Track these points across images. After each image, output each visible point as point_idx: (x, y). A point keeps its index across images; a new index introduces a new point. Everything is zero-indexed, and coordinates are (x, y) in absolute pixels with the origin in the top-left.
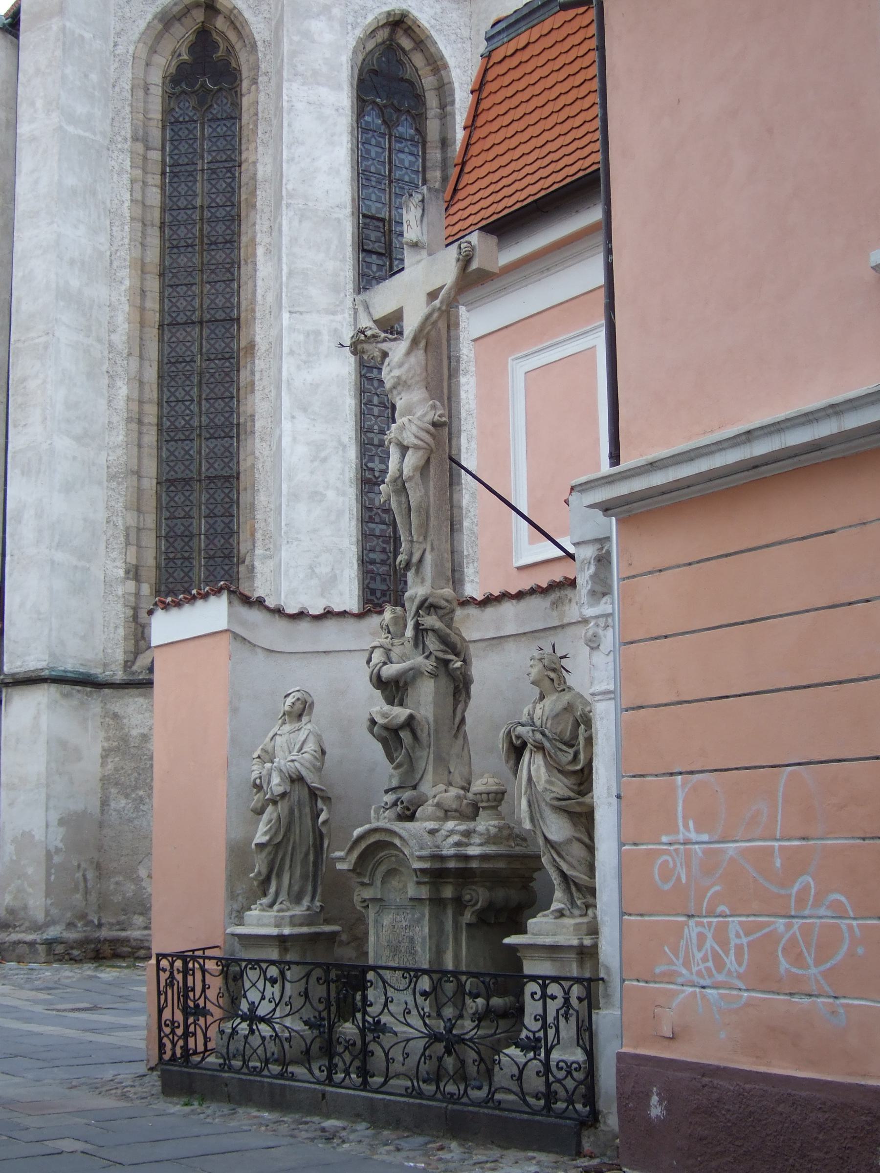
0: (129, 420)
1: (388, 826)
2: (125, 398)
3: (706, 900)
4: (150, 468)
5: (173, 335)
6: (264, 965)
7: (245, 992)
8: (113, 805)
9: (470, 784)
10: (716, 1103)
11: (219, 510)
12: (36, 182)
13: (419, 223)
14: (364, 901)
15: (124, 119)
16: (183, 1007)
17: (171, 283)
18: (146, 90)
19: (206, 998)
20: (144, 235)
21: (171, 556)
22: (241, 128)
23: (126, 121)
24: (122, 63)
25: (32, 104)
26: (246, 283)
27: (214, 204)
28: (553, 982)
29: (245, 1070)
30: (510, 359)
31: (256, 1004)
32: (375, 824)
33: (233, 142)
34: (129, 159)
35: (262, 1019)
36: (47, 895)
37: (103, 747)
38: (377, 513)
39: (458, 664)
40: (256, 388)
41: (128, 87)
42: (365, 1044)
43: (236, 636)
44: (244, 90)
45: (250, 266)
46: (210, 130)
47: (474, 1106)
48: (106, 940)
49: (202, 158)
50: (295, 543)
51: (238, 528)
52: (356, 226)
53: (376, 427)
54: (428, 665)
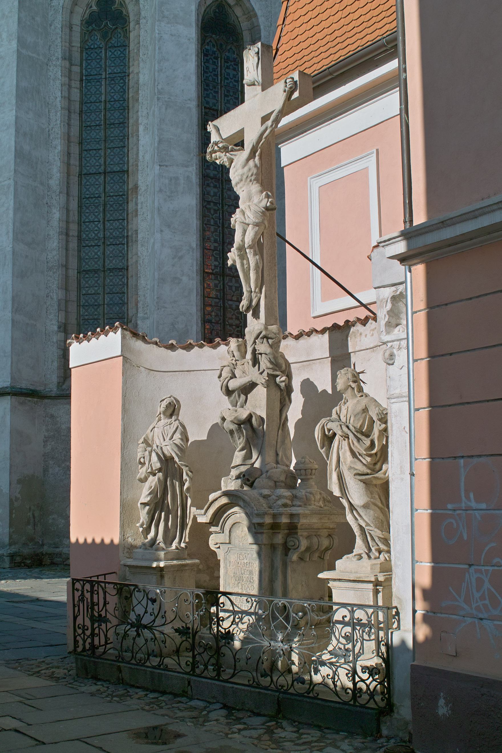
0: (61, 233)
2: (58, 220)
3: (484, 554)
5: (88, 181)
7: (133, 607)
8: (51, 471)
10: (493, 709)
13: (255, 68)
15: (57, 46)
16: (91, 616)
17: (86, 149)
18: (71, 28)
19: (106, 610)
22: (129, 52)
23: (58, 47)
26: (132, 149)
27: (112, 100)
28: (359, 608)
30: (309, 178)
31: (141, 616)
33: (124, 61)
34: (60, 71)
35: (145, 627)
36: (11, 526)
37: (45, 435)
40: (139, 214)
41: (59, 26)
42: (218, 648)
44: (131, 29)
45: (135, 138)
46: (110, 53)
47: (299, 696)
48: (46, 554)
49: (105, 71)
50: (163, 309)
51: (128, 300)
52: (200, 113)
53: (212, 239)
54: (261, 379)
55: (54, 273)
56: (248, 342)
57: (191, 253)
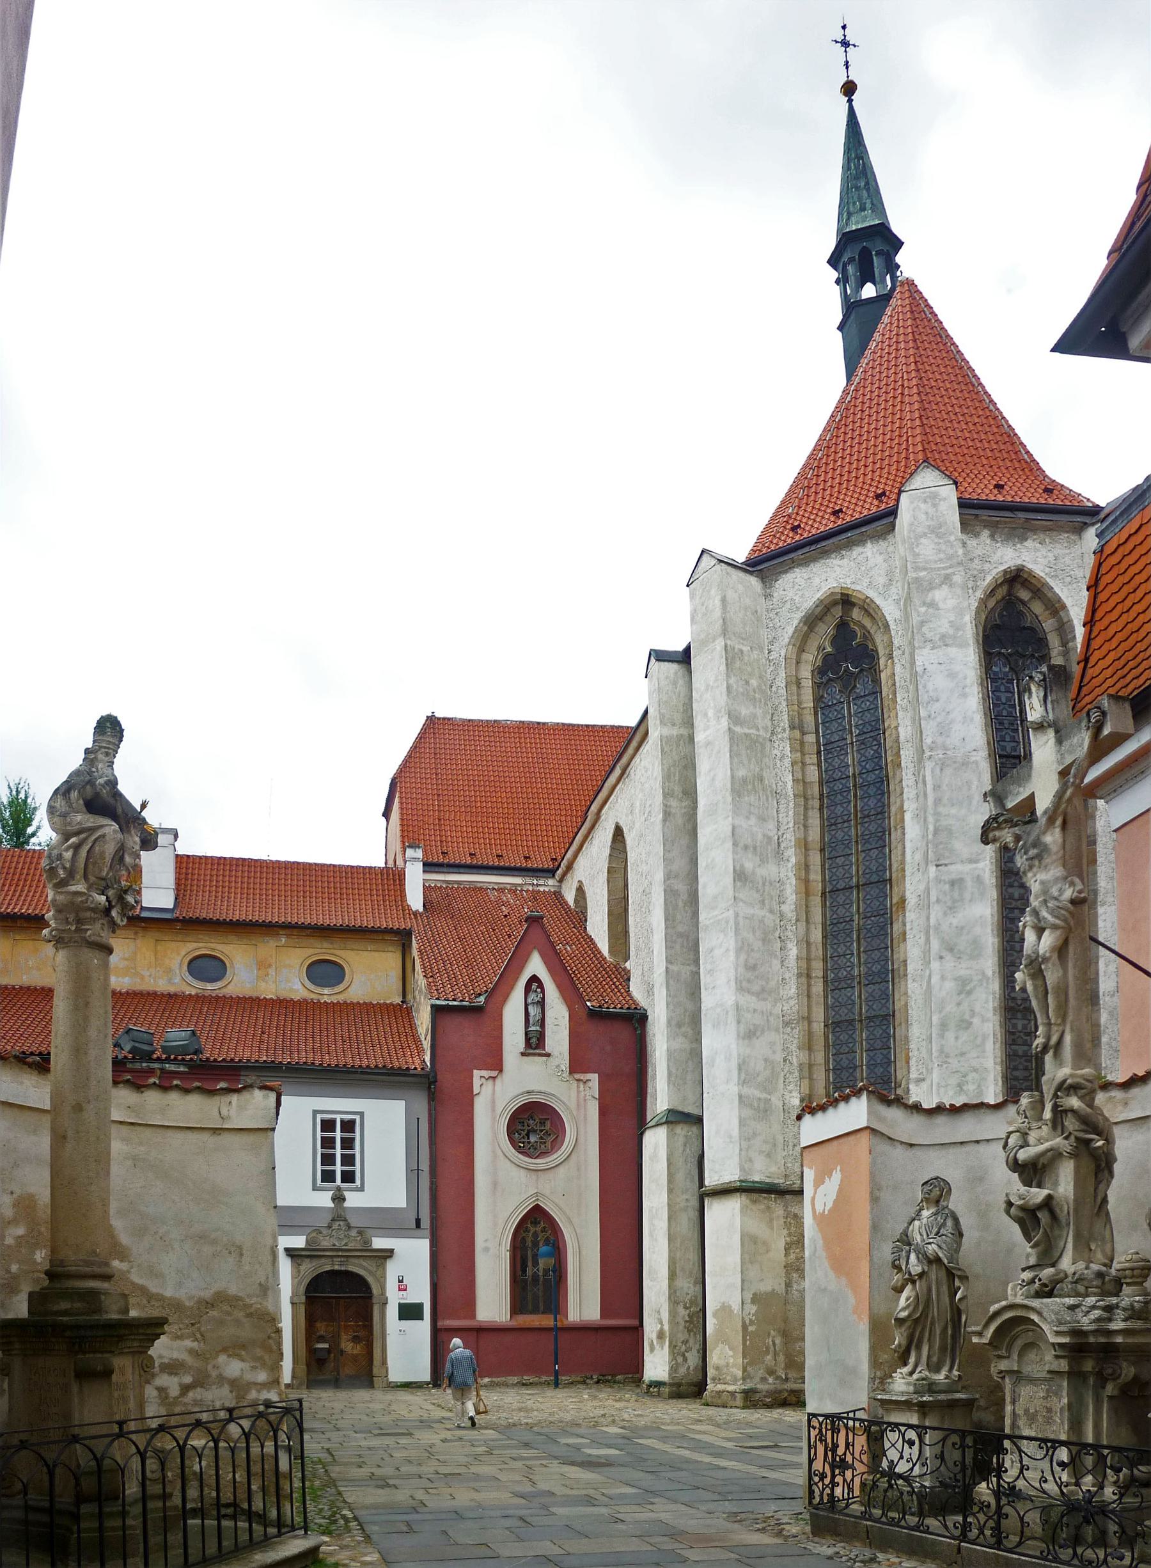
0: (799, 975)
1: (1026, 1302)
4: (819, 1014)
6: (903, 1429)
8: (795, 1286)
9: (1112, 1261)
11: (878, 1044)
12: (713, 779)
14: (1001, 1372)
17: (831, 856)
18: (798, 684)
20: (806, 817)
21: (838, 1085)
22: (882, 699)
24: (776, 665)
25: (706, 715)
26: (896, 847)
29: (884, 1519)
32: (1011, 1300)
36: (744, 1357)
38: (1019, 1037)
39: (1100, 1143)
41: (783, 685)
42: (999, 1507)
43: (873, 1131)
50: (945, 1066)
52: (994, 766)
55: (792, 1029)
56: (1046, 1095)
57: (985, 984)
